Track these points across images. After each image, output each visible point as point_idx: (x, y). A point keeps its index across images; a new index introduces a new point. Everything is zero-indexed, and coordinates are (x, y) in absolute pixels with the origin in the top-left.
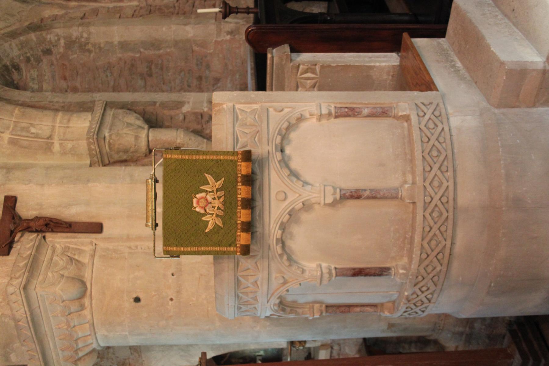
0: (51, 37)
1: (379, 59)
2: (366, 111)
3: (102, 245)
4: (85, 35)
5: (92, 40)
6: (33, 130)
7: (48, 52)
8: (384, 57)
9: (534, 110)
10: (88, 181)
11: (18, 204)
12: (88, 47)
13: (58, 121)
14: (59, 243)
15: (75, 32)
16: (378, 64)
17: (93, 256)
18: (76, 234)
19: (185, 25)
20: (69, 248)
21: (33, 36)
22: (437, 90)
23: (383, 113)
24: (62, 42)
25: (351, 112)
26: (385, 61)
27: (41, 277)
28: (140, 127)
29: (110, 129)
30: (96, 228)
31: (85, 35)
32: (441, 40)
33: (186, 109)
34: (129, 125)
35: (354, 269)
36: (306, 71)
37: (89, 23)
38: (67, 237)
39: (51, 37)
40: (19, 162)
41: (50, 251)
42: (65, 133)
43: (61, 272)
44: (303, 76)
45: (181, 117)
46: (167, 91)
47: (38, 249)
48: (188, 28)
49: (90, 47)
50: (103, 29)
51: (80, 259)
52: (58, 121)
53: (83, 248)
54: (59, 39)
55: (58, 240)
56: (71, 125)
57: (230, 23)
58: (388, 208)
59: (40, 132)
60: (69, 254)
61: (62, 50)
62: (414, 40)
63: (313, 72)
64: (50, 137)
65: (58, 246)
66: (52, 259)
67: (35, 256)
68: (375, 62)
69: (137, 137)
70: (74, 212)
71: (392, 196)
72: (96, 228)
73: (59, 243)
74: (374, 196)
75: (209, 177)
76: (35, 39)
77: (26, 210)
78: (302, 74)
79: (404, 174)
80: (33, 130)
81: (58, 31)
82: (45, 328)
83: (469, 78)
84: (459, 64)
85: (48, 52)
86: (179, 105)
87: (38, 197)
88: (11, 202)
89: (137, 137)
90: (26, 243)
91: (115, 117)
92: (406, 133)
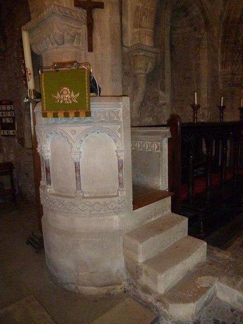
0: (203, 30)
1: (164, 181)
2: (121, 175)
3: (83, 53)
4: (203, 47)
5: (201, 50)
6: (144, 18)
7: (195, 30)
8: (166, 183)
9: (122, 254)
10: (112, 44)
11: (100, 9)
12: (198, 49)
13: (149, 30)
14: (83, 31)
15: (205, 42)
16: (161, 180)
17: (76, 47)
18: (87, 39)
19: (207, 93)
20: (80, 36)
21: (203, 21)
22: (134, 209)
23: (121, 184)
24: (200, 36)
25: (120, 168)
26: (162, 183)
27: (62, 22)
28: (146, 70)
29: (144, 56)
30: (91, 49)
31: (203, 47)
32: (169, 211)
33: (161, 93)
34: (147, 65)
35: (49, 168)
36: (157, 145)
37: (209, 49)
38: (85, 35)
39: (203, 30)
40: (129, 11)
41: (77, 26)
42: (143, 34)
43: (66, 32)
44: (156, 146)
45: (156, 91)
46: (123, 69)
47: (77, 20)
48: (206, 95)
49: (198, 49)
50: (206, 55)
51: (75, 42)
52: (149, 30)
53: (81, 43)
54: (201, 34)
55: (84, 30)
56: (147, 37)
57: (208, 113)
58: (73, 185)
59: (143, 21)
60: (76, 36)
61: (196, 36)
62: (170, 197)
63: (157, 149)
64: (140, 26)
65: (81, 31)
66: (73, 28)
67: (73, 18)
68: (162, 180)
69: (140, 68)
70: (97, 38)
71: (79, 187)
72: (91, 49)
73: (83, 31)
74: (78, 179)
75: (78, 94)
76: (201, 23)
77: (97, 13)
78: (156, 144)
79: (89, 193)
80: (144, 18)
81: (206, 33)
82: (86, 43)
83: (143, 224)
84: (153, 219)
85: (195, 30)
86: (163, 90)
87: (105, 18)
88: (101, 6)
89: (140, 68)
90: (81, 13)
91: (151, 58)
92: (111, 194)
